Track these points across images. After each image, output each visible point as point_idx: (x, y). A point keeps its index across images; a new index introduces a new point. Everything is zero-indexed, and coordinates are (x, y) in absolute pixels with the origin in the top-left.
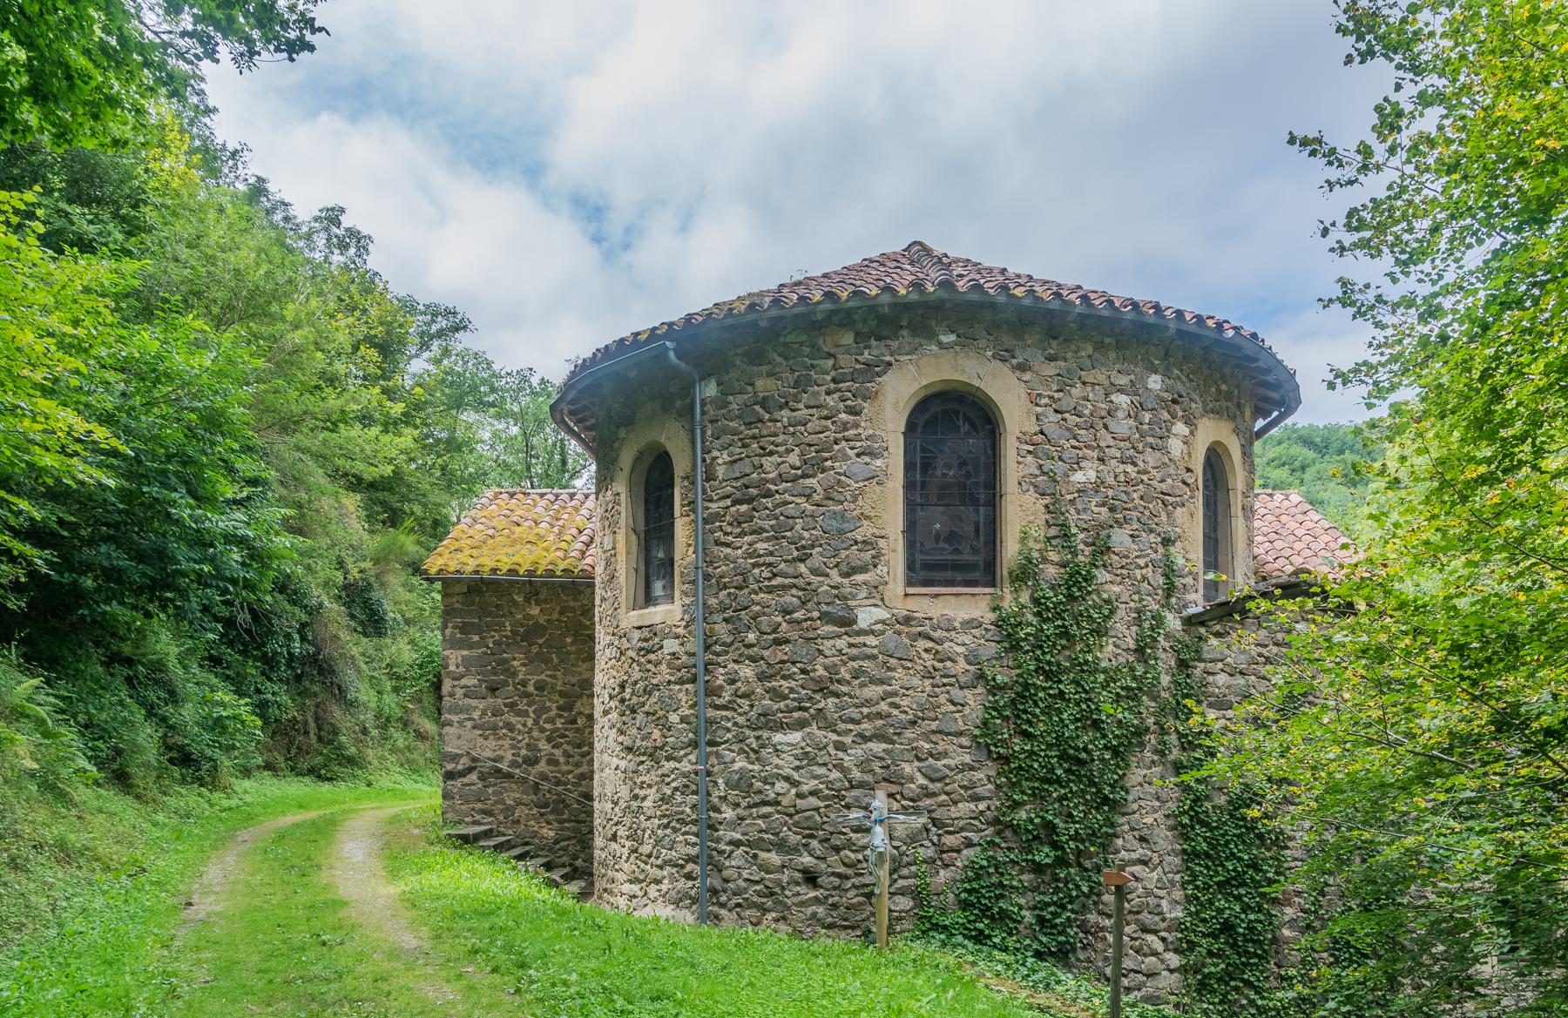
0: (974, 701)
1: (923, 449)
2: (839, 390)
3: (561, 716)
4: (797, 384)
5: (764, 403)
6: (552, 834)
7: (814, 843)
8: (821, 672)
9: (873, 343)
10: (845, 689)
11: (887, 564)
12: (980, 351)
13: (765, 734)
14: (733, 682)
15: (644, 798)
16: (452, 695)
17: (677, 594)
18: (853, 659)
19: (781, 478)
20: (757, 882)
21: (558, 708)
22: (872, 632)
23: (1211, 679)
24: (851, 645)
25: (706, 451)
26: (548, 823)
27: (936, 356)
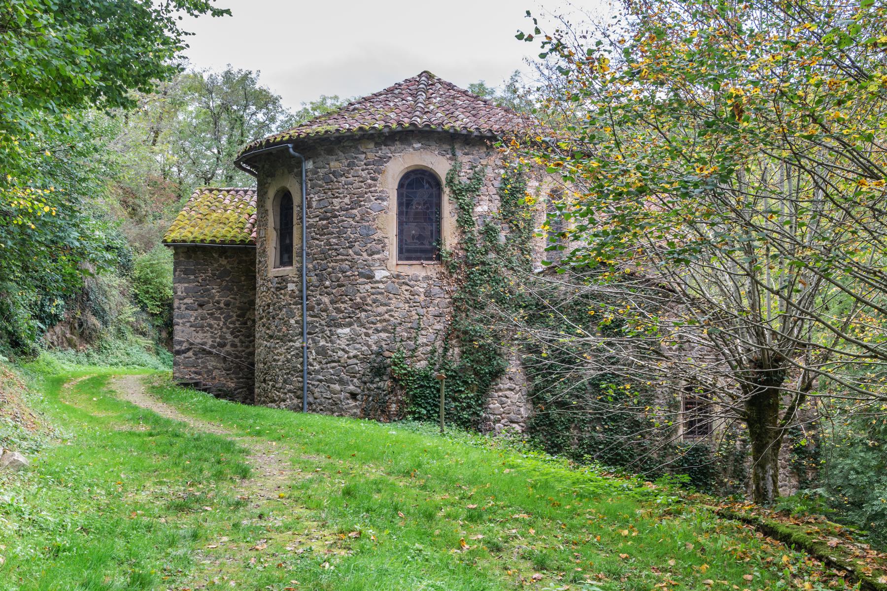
1: (407, 196)
3: (238, 320)
4: (349, 165)
5: (334, 173)
6: (233, 385)
7: (355, 380)
8: (358, 300)
9: (383, 147)
10: (369, 308)
11: (389, 250)
13: (333, 329)
14: (319, 304)
15: (279, 360)
16: (179, 308)
17: (294, 262)
18: (373, 294)
19: (341, 209)
22: (382, 282)
24: (372, 288)
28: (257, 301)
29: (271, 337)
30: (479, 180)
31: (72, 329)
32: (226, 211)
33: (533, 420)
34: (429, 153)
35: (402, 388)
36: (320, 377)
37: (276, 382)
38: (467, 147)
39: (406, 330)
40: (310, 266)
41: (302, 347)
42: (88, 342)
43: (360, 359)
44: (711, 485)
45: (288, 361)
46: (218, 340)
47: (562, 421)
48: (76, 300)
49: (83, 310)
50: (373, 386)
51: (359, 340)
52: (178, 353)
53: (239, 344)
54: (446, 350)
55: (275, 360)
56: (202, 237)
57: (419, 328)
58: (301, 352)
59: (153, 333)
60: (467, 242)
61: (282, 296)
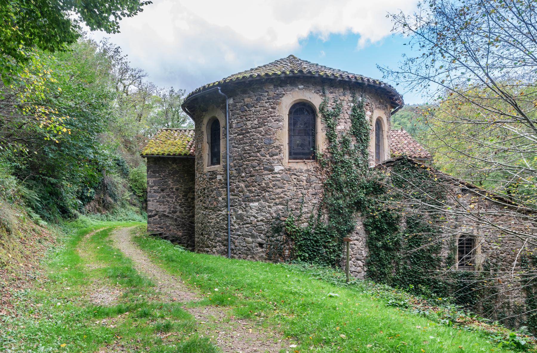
1: (294, 119)
5: (247, 105)
6: (181, 234)
7: (262, 235)
8: (264, 185)
9: (279, 88)
10: (271, 190)
11: (283, 153)
12: (310, 90)
13: (247, 203)
14: (237, 188)
15: (211, 222)
22: (279, 173)
24: (273, 177)
28: (196, 187)
29: (206, 208)
30: (339, 109)
31: (99, 203)
32: (175, 139)
33: (369, 258)
34: (308, 91)
35: (292, 240)
36: (239, 233)
37: (210, 235)
38: (332, 88)
39: (294, 204)
40: (232, 164)
41: (227, 215)
42: (107, 210)
43: (265, 222)
44: (477, 297)
45: (218, 223)
46: (172, 209)
47: (386, 259)
48: (101, 189)
49: (104, 194)
50: (273, 239)
51: (264, 210)
52: (150, 216)
54: (319, 216)
55: (209, 222)
56: (162, 152)
57: (302, 202)
58: (226, 218)
59: (139, 205)
60: (332, 149)
61: (213, 183)
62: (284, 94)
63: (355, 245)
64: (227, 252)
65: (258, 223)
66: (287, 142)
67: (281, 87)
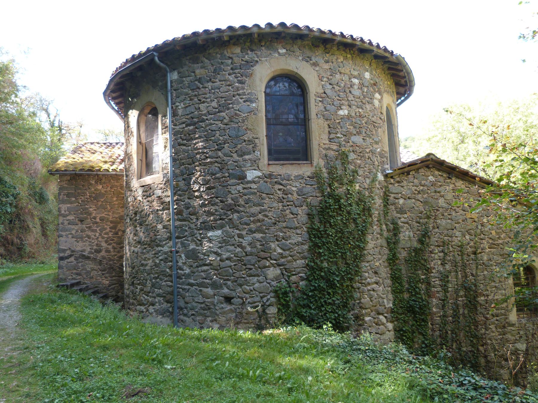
0: (302, 212)
2: (235, 73)
3: (111, 231)
4: (215, 71)
5: (200, 80)
6: (107, 282)
7: (229, 283)
8: (230, 201)
9: (249, 52)
10: (241, 209)
11: (260, 151)
12: (297, 57)
14: (188, 208)
15: (147, 265)
19: (209, 113)
20: (202, 303)
21: (110, 228)
23: (397, 201)
24: (244, 188)
25: (173, 103)
26: (106, 278)
27: (277, 58)
36: (192, 281)
37: (144, 285)
45: (156, 265)
53: (112, 250)
55: (142, 265)
62: (257, 62)
63: (374, 290)
64: (172, 313)
65: (223, 264)
66: (265, 134)
67: (252, 50)
